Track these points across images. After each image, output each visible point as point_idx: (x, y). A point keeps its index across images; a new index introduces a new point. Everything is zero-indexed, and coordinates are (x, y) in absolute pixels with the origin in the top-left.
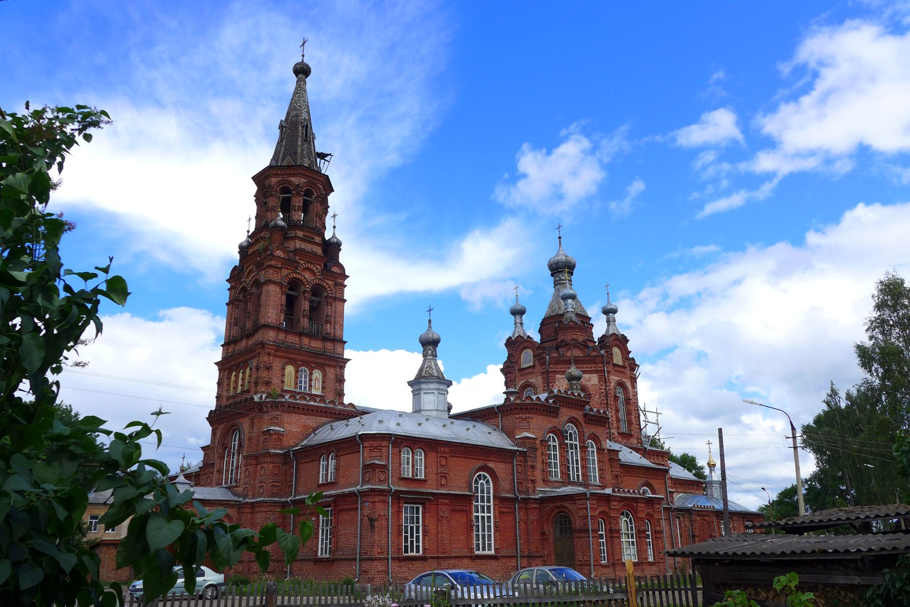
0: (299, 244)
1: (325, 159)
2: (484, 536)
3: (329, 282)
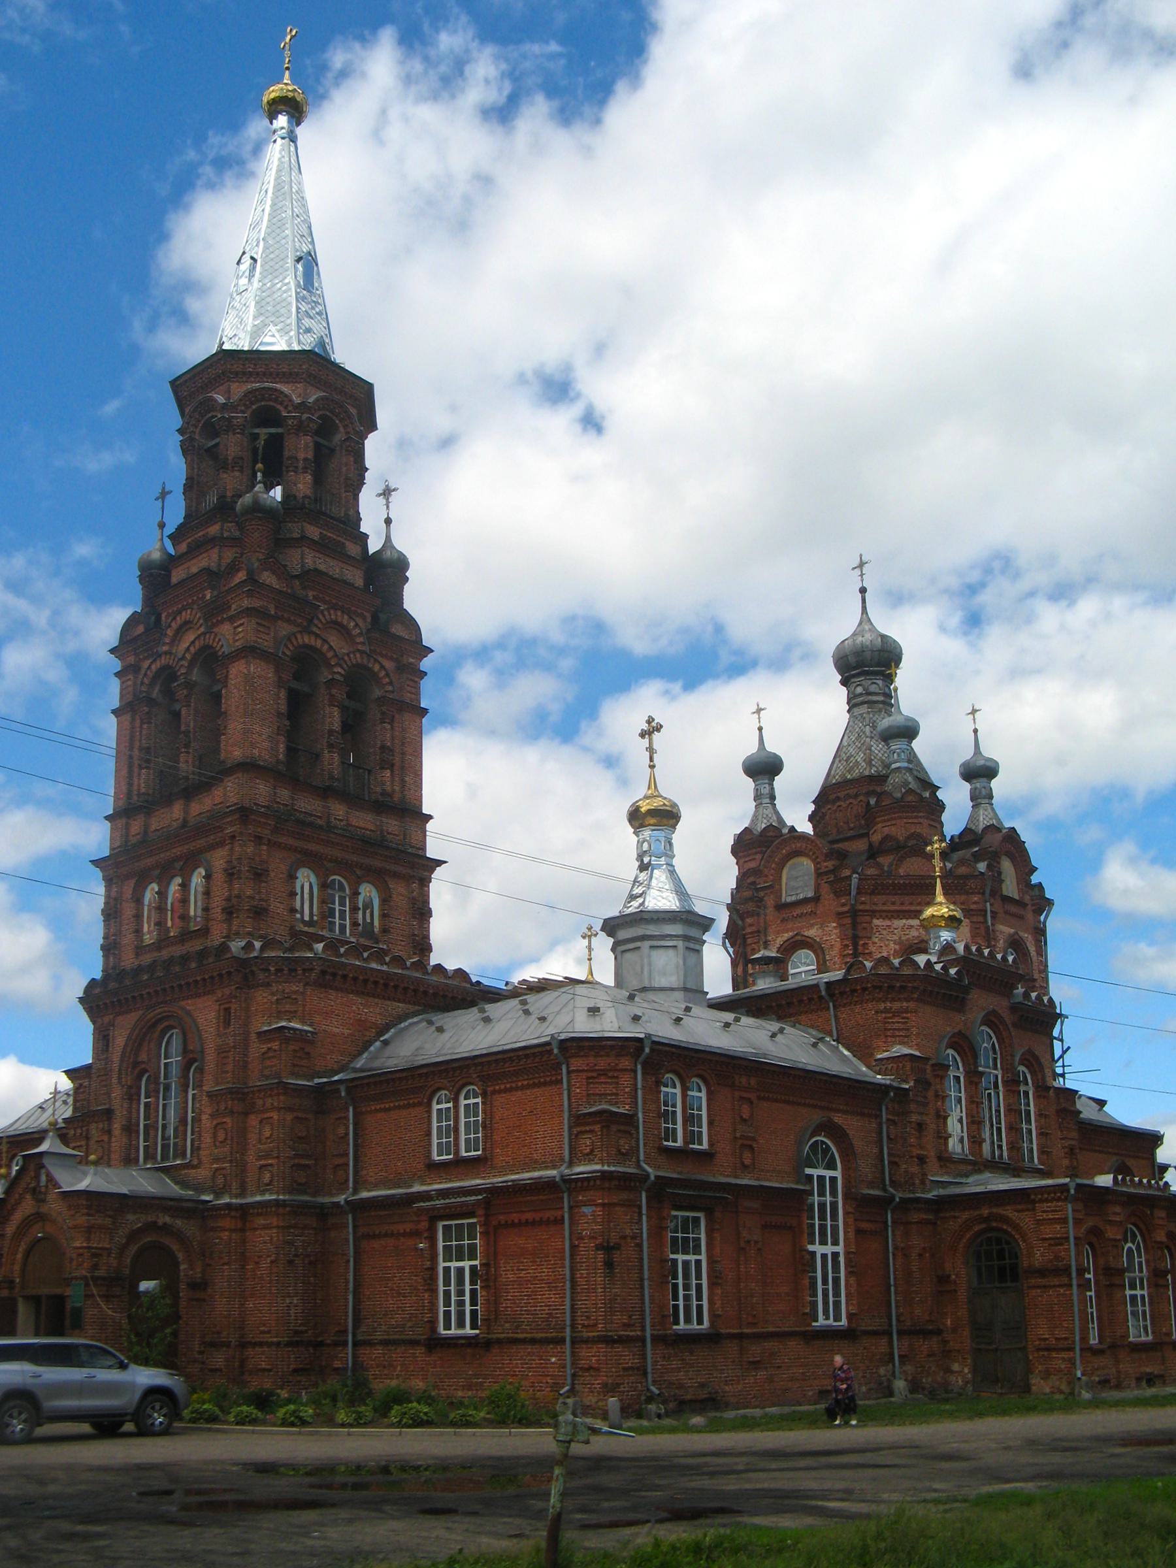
0: (312, 559)
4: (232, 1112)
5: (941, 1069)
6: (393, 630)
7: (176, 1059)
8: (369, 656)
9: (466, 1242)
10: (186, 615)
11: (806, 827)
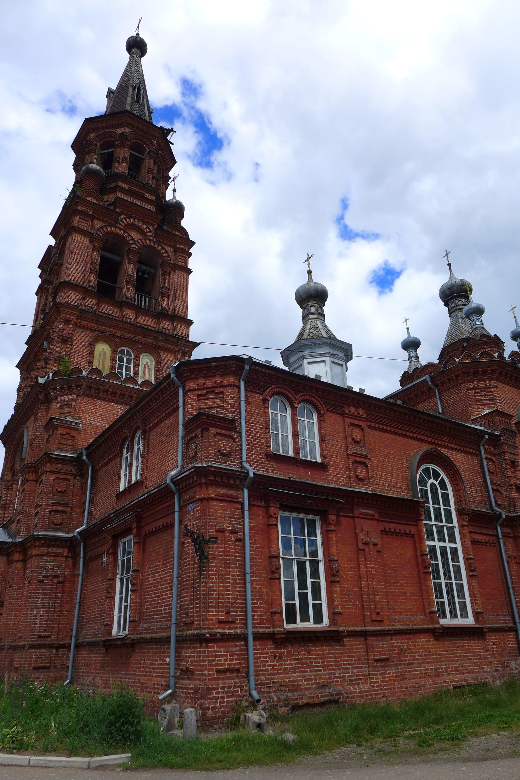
2: (449, 587)
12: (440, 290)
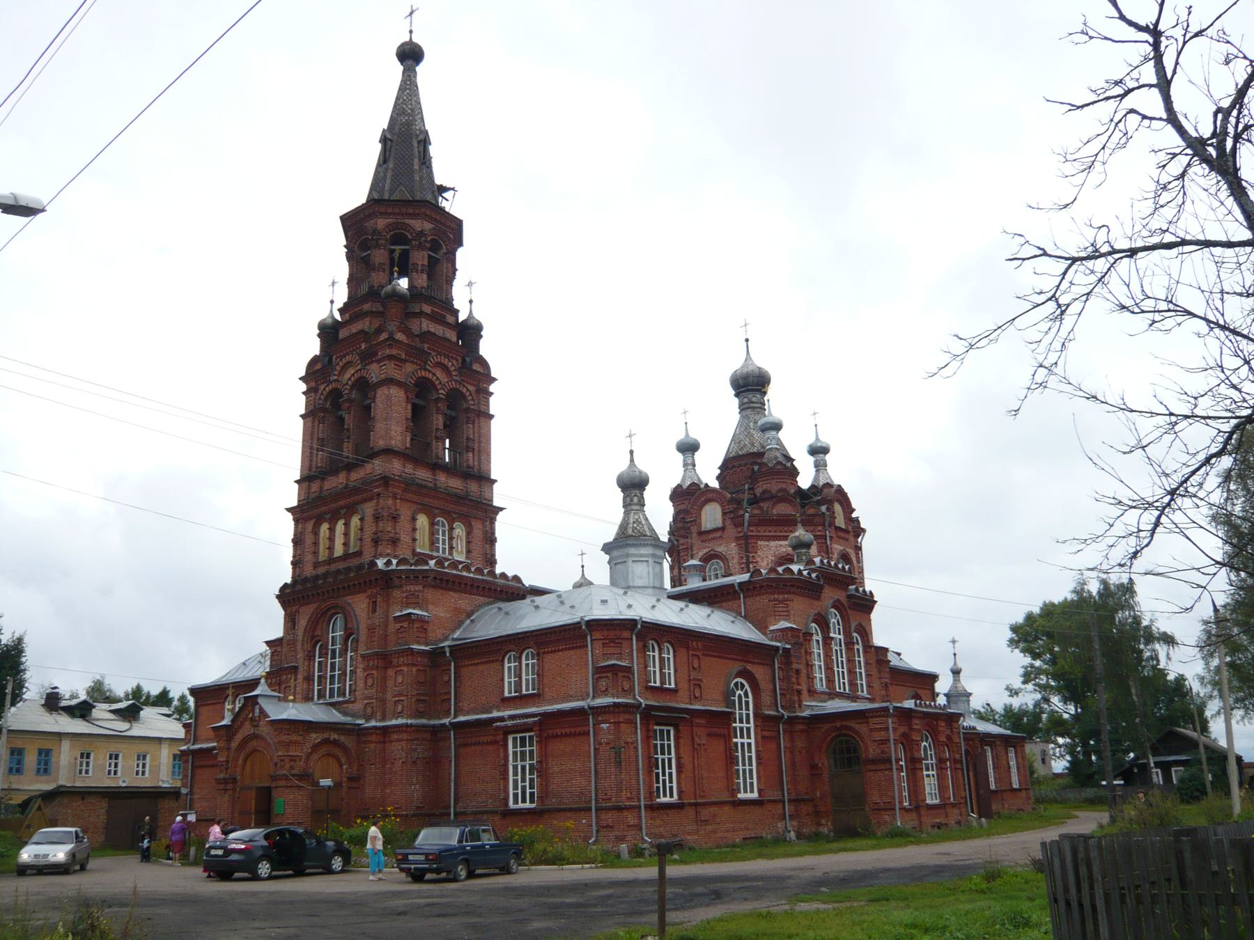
0: (427, 326)
1: (443, 195)
2: (744, 771)
3: (471, 388)
4: (377, 667)
5: (808, 635)
6: (474, 368)
7: (339, 633)
8: (460, 383)
9: (519, 749)
10: (348, 358)
11: (715, 484)
12: (732, 376)
